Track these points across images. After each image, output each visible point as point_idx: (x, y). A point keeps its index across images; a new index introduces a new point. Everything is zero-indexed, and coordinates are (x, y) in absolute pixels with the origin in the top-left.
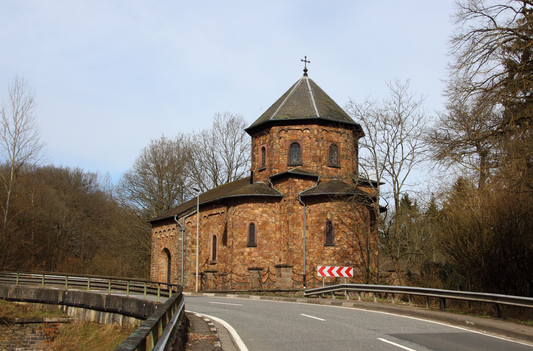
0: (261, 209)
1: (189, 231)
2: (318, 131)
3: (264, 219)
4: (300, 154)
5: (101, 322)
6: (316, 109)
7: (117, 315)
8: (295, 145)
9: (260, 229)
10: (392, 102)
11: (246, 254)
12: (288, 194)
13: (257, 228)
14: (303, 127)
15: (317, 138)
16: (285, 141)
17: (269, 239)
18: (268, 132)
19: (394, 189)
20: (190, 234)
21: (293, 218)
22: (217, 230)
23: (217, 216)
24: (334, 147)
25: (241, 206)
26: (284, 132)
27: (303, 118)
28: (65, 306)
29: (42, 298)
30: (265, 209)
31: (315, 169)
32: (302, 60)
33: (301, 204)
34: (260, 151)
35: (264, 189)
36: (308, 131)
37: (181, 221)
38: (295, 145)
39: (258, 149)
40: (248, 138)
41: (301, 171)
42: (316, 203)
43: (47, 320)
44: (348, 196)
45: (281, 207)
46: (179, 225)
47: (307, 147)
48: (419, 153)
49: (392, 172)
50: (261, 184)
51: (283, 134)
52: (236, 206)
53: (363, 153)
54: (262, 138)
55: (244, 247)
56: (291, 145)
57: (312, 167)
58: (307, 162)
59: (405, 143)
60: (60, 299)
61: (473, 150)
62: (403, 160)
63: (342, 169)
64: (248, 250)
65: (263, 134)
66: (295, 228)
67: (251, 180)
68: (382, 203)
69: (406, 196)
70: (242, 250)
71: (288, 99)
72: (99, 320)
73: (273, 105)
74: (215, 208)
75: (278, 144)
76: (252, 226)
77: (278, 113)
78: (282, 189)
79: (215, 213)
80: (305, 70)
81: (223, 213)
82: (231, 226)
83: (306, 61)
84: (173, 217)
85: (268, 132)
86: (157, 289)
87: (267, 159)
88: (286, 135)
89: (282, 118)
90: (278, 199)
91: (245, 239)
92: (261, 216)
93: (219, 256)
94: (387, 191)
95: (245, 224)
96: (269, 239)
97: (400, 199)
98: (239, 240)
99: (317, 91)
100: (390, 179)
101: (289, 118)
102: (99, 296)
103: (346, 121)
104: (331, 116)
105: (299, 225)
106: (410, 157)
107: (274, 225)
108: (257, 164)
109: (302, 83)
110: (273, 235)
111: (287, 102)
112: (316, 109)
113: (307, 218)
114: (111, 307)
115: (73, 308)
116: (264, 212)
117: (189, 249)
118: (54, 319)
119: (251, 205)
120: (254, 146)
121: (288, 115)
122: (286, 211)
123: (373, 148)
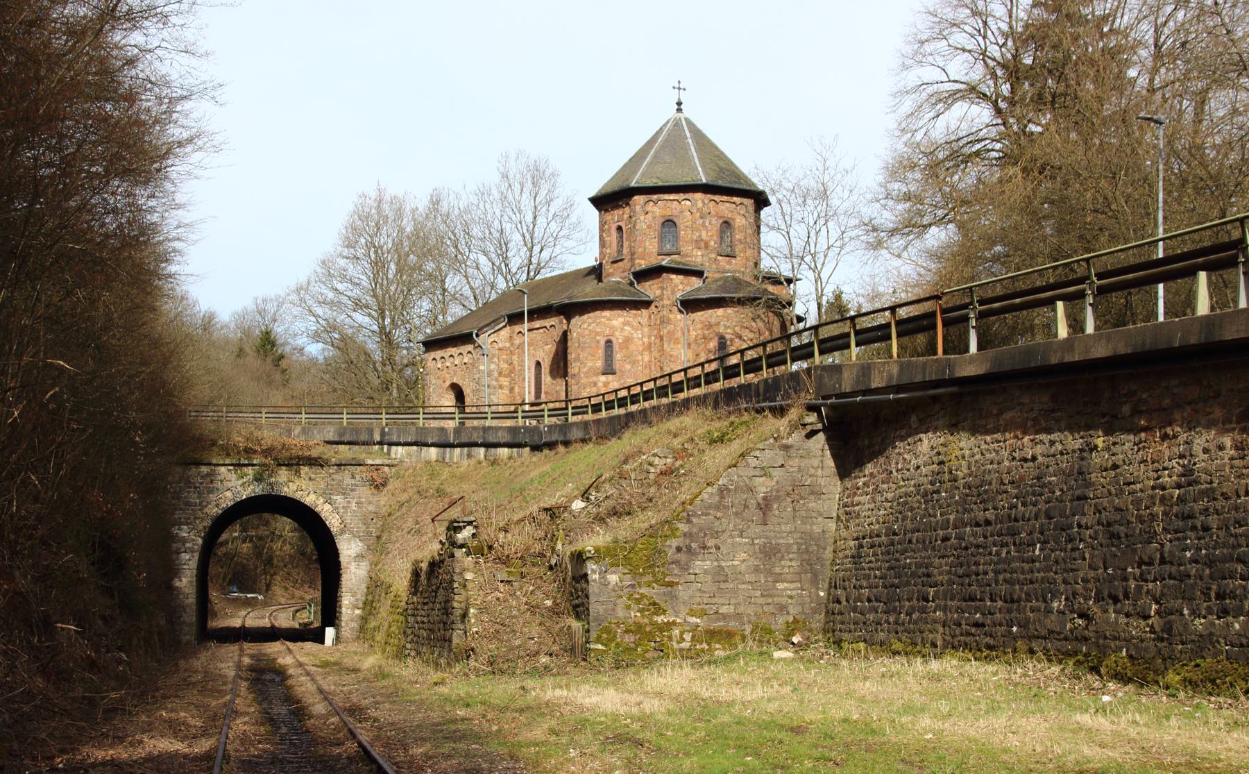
0: (621, 320)
1: (494, 356)
2: (703, 202)
3: (626, 334)
4: (676, 237)
5: (447, 460)
6: (700, 169)
7: (475, 449)
8: (669, 223)
9: (621, 349)
10: (814, 169)
11: (600, 384)
12: (661, 298)
13: (616, 347)
14: (681, 196)
15: (701, 213)
16: (654, 218)
17: (634, 363)
18: (628, 204)
19: (817, 290)
20: (496, 360)
21: (668, 332)
22: (546, 353)
23: (541, 331)
24: (727, 224)
25: (591, 315)
26: (651, 203)
27: (682, 183)
28: (386, 447)
29: (347, 438)
30: (627, 318)
31: (699, 260)
32: (674, 88)
33: (681, 311)
34: (614, 234)
35: (624, 290)
36: (688, 203)
37: (484, 339)
38: (669, 223)
39: (610, 228)
40: (593, 212)
41: (679, 263)
42: (703, 309)
43: (370, 462)
44: (755, 299)
45: (650, 317)
46: (480, 346)
47: (687, 227)
48: (851, 239)
49: (813, 266)
50: (618, 283)
51: (650, 206)
52: (583, 314)
53: (770, 239)
54: (616, 212)
55: (597, 375)
56: (663, 223)
57: (696, 258)
58: (685, 249)
59: (830, 224)
60: (377, 438)
61: (354, 625)
62: (829, 248)
63: (738, 258)
64: (603, 378)
65: (618, 207)
66: (672, 346)
67: (596, 272)
68: (799, 309)
69: (838, 297)
70: (595, 379)
71: (656, 152)
72: (444, 459)
73: (630, 160)
74: (538, 319)
75: (643, 222)
76: (609, 342)
77: (643, 175)
78: (650, 289)
79: (538, 326)
80: (679, 104)
81: (552, 326)
82: (577, 345)
83: (679, 89)
84: (471, 334)
85: (628, 204)
86: (523, 418)
87: (626, 244)
88: (656, 209)
89: (649, 182)
90: (647, 304)
91: (600, 364)
92: (622, 329)
93: (546, 393)
94: (808, 292)
95: (598, 342)
96: (634, 363)
97: (824, 303)
98: (590, 364)
99: (698, 135)
100: (811, 275)
101: (660, 184)
102: (442, 429)
103: (744, 187)
104: (722, 178)
105: (677, 341)
106: (838, 244)
107: (641, 342)
108: (608, 251)
109: (675, 125)
110: (640, 358)
111: (655, 157)
112: (700, 169)
113: (689, 331)
114: (464, 439)
115: (400, 448)
116: (626, 323)
117: (494, 383)
118: (378, 462)
119: (607, 313)
120: (602, 224)
121: (658, 178)
122: (658, 322)
123: (788, 233)
